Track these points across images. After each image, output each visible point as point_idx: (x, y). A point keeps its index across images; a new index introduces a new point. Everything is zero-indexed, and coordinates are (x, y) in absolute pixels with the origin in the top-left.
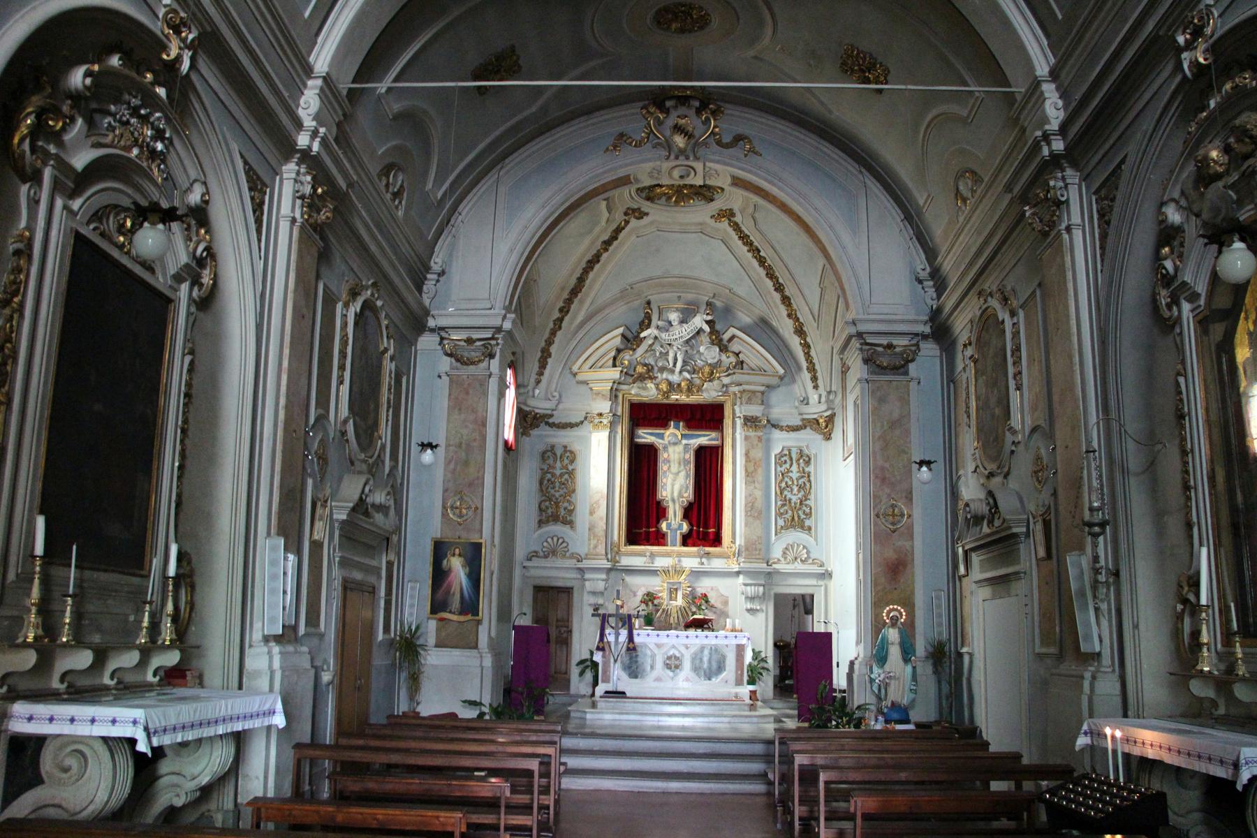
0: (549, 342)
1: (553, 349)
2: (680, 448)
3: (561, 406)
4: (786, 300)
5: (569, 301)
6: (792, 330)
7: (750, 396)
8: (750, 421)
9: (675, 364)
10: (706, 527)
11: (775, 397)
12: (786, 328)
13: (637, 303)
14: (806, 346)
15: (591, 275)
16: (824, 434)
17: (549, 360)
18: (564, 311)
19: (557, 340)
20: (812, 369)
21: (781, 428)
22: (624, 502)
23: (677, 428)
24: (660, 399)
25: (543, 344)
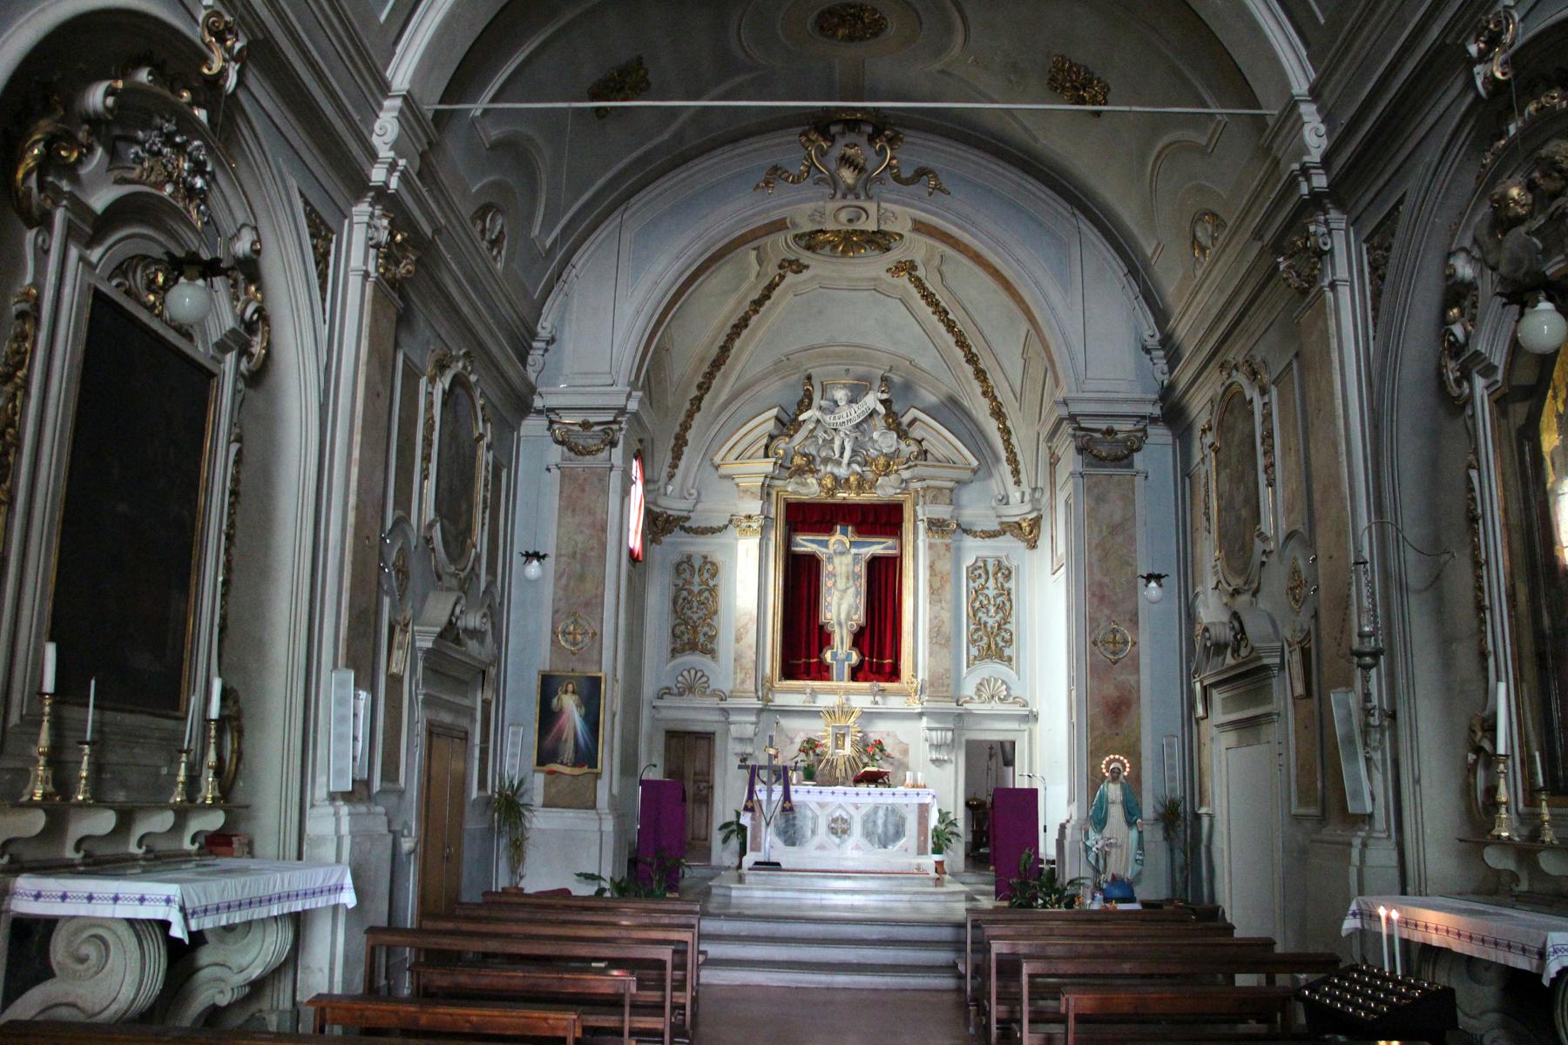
0: (685, 427)
1: (690, 435)
2: (848, 559)
3: (699, 507)
4: (981, 375)
5: (710, 376)
6: (988, 412)
7: (936, 494)
8: (936, 526)
9: (842, 454)
10: (881, 657)
11: (966, 495)
12: (980, 409)
13: (795, 378)
14: (1006, 432)
15: (737, 343)
16: (1028, 541)
17: (685, 449)
18: (704, 387)
19: (695, 424)
20: (1013, 460)
21: (975, 534)
22: (779, 626)
23: (845, 533)
24: (823, 497)
25: (677, 429)
